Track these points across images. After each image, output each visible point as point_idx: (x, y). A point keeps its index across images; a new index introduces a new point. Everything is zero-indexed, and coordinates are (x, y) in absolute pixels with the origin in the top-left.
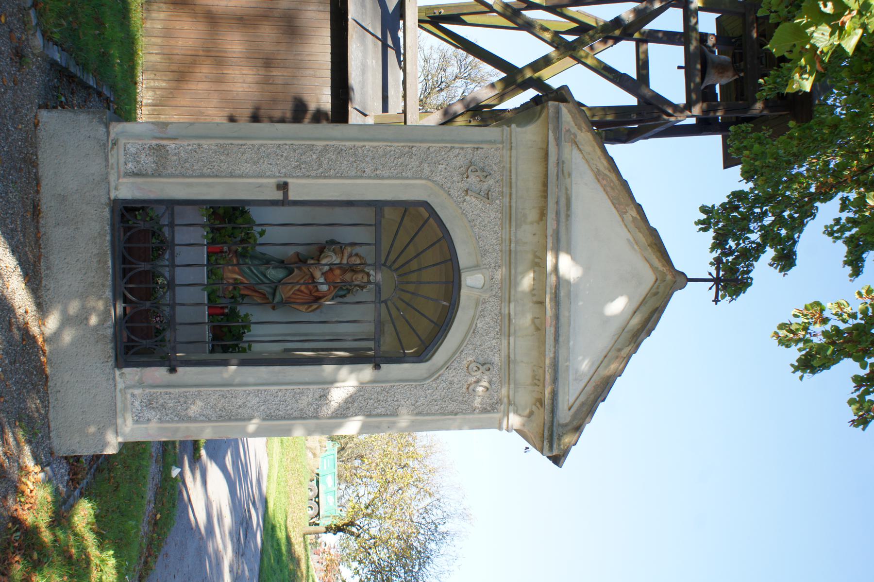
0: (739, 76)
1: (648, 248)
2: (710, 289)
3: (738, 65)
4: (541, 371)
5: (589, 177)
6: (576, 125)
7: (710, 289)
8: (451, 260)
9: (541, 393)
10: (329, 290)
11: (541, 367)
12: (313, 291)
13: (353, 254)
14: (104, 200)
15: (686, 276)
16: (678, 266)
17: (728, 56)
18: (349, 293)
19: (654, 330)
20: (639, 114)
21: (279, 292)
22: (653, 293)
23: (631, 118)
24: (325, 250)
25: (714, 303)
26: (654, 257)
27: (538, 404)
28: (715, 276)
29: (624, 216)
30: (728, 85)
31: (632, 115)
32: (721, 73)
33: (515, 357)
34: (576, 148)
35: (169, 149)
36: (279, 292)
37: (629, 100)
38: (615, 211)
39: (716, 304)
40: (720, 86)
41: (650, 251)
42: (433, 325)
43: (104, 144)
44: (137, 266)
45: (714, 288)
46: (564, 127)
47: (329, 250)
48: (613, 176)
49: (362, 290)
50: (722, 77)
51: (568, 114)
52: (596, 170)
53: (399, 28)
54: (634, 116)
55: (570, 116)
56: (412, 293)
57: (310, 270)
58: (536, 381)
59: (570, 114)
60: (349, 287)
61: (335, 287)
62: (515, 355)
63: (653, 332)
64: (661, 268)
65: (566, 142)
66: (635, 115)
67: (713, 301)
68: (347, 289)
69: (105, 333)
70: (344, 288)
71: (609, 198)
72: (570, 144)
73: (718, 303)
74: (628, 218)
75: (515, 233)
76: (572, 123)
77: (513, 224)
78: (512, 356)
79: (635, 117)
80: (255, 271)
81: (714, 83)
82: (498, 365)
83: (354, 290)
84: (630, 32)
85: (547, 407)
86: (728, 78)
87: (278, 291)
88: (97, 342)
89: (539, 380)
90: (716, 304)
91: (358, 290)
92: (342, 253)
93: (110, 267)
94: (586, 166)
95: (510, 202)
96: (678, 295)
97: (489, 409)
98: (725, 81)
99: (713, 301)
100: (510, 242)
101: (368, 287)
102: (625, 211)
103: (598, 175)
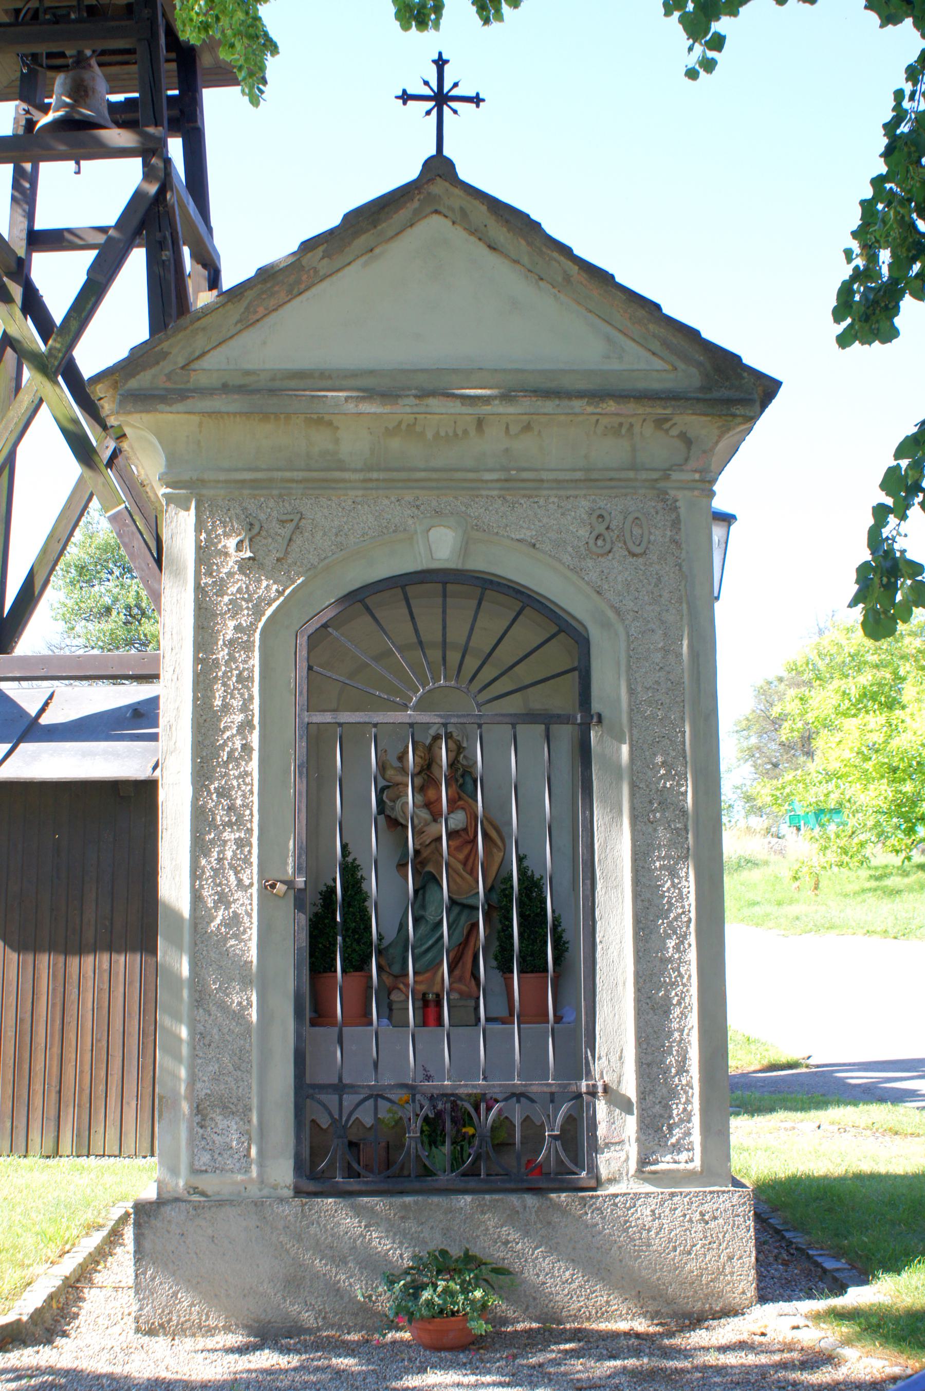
0: (91, 57)
1: (379, 228)
2: (455, 112)
3: (71, 61)
4: (604, 421)
5: (250, 338)
6: (158, 363)
7: (455, 112)
8: (403, 587)
9: (644, 420)
10: (463, 808)
11: (598, 421)
12: (466, 837)
13: (399, 765)
14: (291, 1209)
15: (432, 157)
16: (411, 172)
17: (54, 79)
18: (470, 773)
19: (528, 216)
20: (161, 245)
21: (466, 898)
22: (462, 219)
23: (169, 260)
24: (393, 816)
25: (481, 104)
26: (396, 216)
27: (667, 426)
28: (433, 103)
29: (322, 273)
30: (109, 78)
31: (164, 258)
32: (86, 91)
33: (580, 470)
34: (199, 362)
35: (203, 1093)
36: (466, 898)
37: (137, 259)
38: (314, 290)
39: (483, 100)
40: (111, 93)
41: (384, 225)
42: (448, 599)
43: (195, 1209)
44: (412, 1151)
45: (453, 104)
46: (162, 382)
47: (393, 809)
48: (250, 295)
49: (464, 748)
50: (94, 90)
51: (138, 377)
52: (239, 325)
53: (288, 856)
54: (166, 254)
55: (142, 374)
56: (421, 643)
57: (427, 843)
58: (623, 431)
59: (138, 373)
60: (460, 772)
61: (460, 798)
62: (574, 470)
63: (533, 217)
64: (416, 204)
65: (188, 381)
66: (163, 253)
67: (478, 106)
68: (463, 776)
69: (534, 1210)
70: (461, 781)
71: (289, 301)
72: (192, 374)
73: (481, 96)
74: (324, 266)
75: (355, 470)
76: (153, 371)
77: (337, 475)
78: (579, 475)
79: (167, 253)
80: (430, 942)
81: (106, 105)
82: (594, 501)
83: (465, 763)
84: (13, 265)
85: (668, 411)
86: (98, 77)
87: (465, 901)
88: (549, 1223)
89: (621, 425)
90: (483, 100)
91: (465, 757)
92: (398, 784)
93: (416, 1198)
94: (232, 343)
95: (297, 482)
96: (465, 173)
97: (674, 516)
98: (101, 84)
99: (478, 106)
100: (371, 480)
101: (459, 738)
102: (312, 272)
103: (248, 323)
